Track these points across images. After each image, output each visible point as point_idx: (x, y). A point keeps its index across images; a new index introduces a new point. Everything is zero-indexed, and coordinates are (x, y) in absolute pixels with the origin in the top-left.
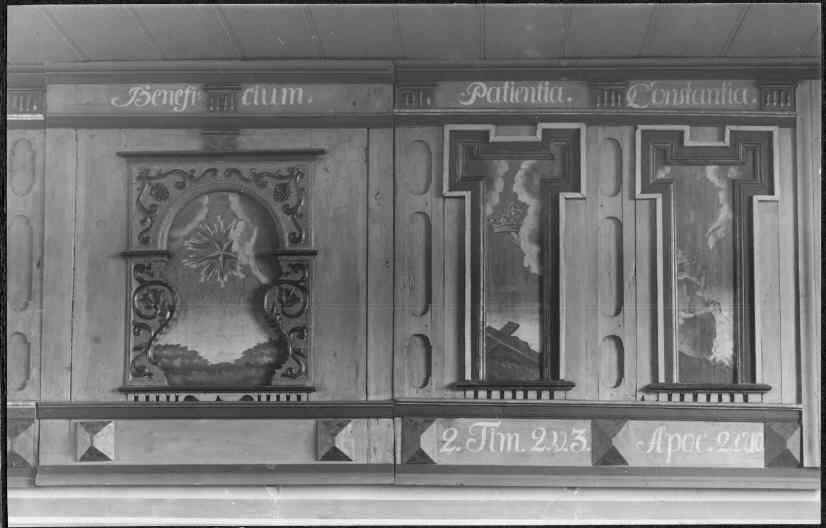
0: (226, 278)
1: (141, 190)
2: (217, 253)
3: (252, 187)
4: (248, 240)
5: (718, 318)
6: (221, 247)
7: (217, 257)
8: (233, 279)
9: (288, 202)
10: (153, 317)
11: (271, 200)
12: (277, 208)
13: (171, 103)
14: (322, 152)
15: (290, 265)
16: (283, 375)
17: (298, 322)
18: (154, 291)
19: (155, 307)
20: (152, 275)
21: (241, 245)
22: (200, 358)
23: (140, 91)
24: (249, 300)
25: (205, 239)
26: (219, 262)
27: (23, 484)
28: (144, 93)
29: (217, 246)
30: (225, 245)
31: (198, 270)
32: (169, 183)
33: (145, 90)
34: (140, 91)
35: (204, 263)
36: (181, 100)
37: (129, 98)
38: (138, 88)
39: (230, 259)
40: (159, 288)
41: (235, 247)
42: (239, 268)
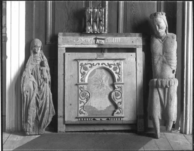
0: (102, 89)
1: (81, 68)
2: (99, 83)
3: (108, 67)
4: (107, 79)
5: (159, 132)
6: (101, 81)
7: (100, 84)
8: (104, 90)
9: (117, 71)
10: (84, 99)
11: (113, 71)
12: (114, 72)
13: (88, 41)
14: (125, 59)
15: (117, 87)
16: (116, 113)
17: (120, 100)
18: (85, 93)
19: (85, 97)
20: (84, 89)
21: (105, 81)
22: (96, 109)
23: (81, 38)
24: (156, 54)
25: (96, 79)
26: (100, 85)
27: (144, 44)
28: (82, 39)
29: (100, 82)
30: (101, 81)
31: (95, 87)
32: (88, 66)
33: (82, 38)
34: (81, 38)
35: (96, 86)
36: (91, 40)
37: (78, 40)
38: (80, 38)
39: (102, 85)
40: (86, 92)
41: (104, 82)
42: (105, 87)
